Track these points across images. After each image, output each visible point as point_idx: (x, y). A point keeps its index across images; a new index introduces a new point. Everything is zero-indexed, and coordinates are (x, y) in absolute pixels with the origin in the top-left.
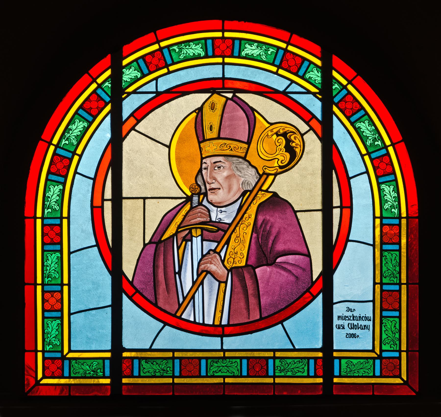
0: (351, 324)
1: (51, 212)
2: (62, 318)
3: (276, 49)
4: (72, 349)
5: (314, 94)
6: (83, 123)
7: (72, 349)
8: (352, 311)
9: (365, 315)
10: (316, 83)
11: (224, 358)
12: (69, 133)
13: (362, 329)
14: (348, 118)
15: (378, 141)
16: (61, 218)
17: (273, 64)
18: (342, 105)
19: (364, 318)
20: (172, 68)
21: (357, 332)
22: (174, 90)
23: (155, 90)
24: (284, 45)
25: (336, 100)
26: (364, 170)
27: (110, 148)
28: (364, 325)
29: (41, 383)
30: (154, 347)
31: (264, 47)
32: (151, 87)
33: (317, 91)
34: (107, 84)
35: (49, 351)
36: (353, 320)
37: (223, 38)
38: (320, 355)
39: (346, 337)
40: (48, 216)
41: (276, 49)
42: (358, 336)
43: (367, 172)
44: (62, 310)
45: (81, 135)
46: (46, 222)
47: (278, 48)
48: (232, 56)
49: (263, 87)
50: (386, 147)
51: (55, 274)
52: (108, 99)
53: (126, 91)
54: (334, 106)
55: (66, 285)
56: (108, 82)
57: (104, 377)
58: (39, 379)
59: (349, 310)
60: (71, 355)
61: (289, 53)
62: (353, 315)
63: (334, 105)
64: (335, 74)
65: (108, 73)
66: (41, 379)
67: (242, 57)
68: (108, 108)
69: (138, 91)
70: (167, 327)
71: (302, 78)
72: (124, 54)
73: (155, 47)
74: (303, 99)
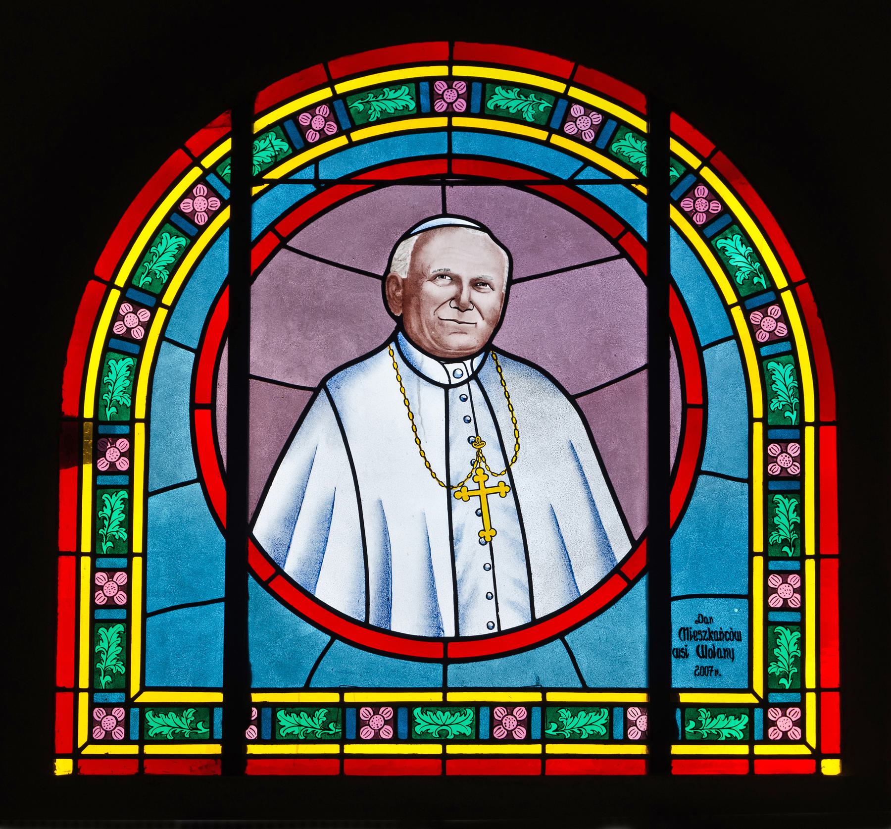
0: (702, 646)
4: (148, 684)
7: (148, 684)
8: (707, 623)
9: (731, 629)
11: (445, 705)
12: (103, 526)
13: (721, 657)
19: (728, 636)
21: (716, 663)
22: (361, 177)
28: (724, 649)
32: (309, 173)
36: (710, 639)
40: (224, 177)
52: (226, 194)
54: (672, 208)
57: (211, 741)
58: (80, 745)
59: (701, 619)
60: (148, 697)
62: (709, 629)
63: (671, 206)
64: (675, 147)
65: (226, 146)
69: (292, 178)
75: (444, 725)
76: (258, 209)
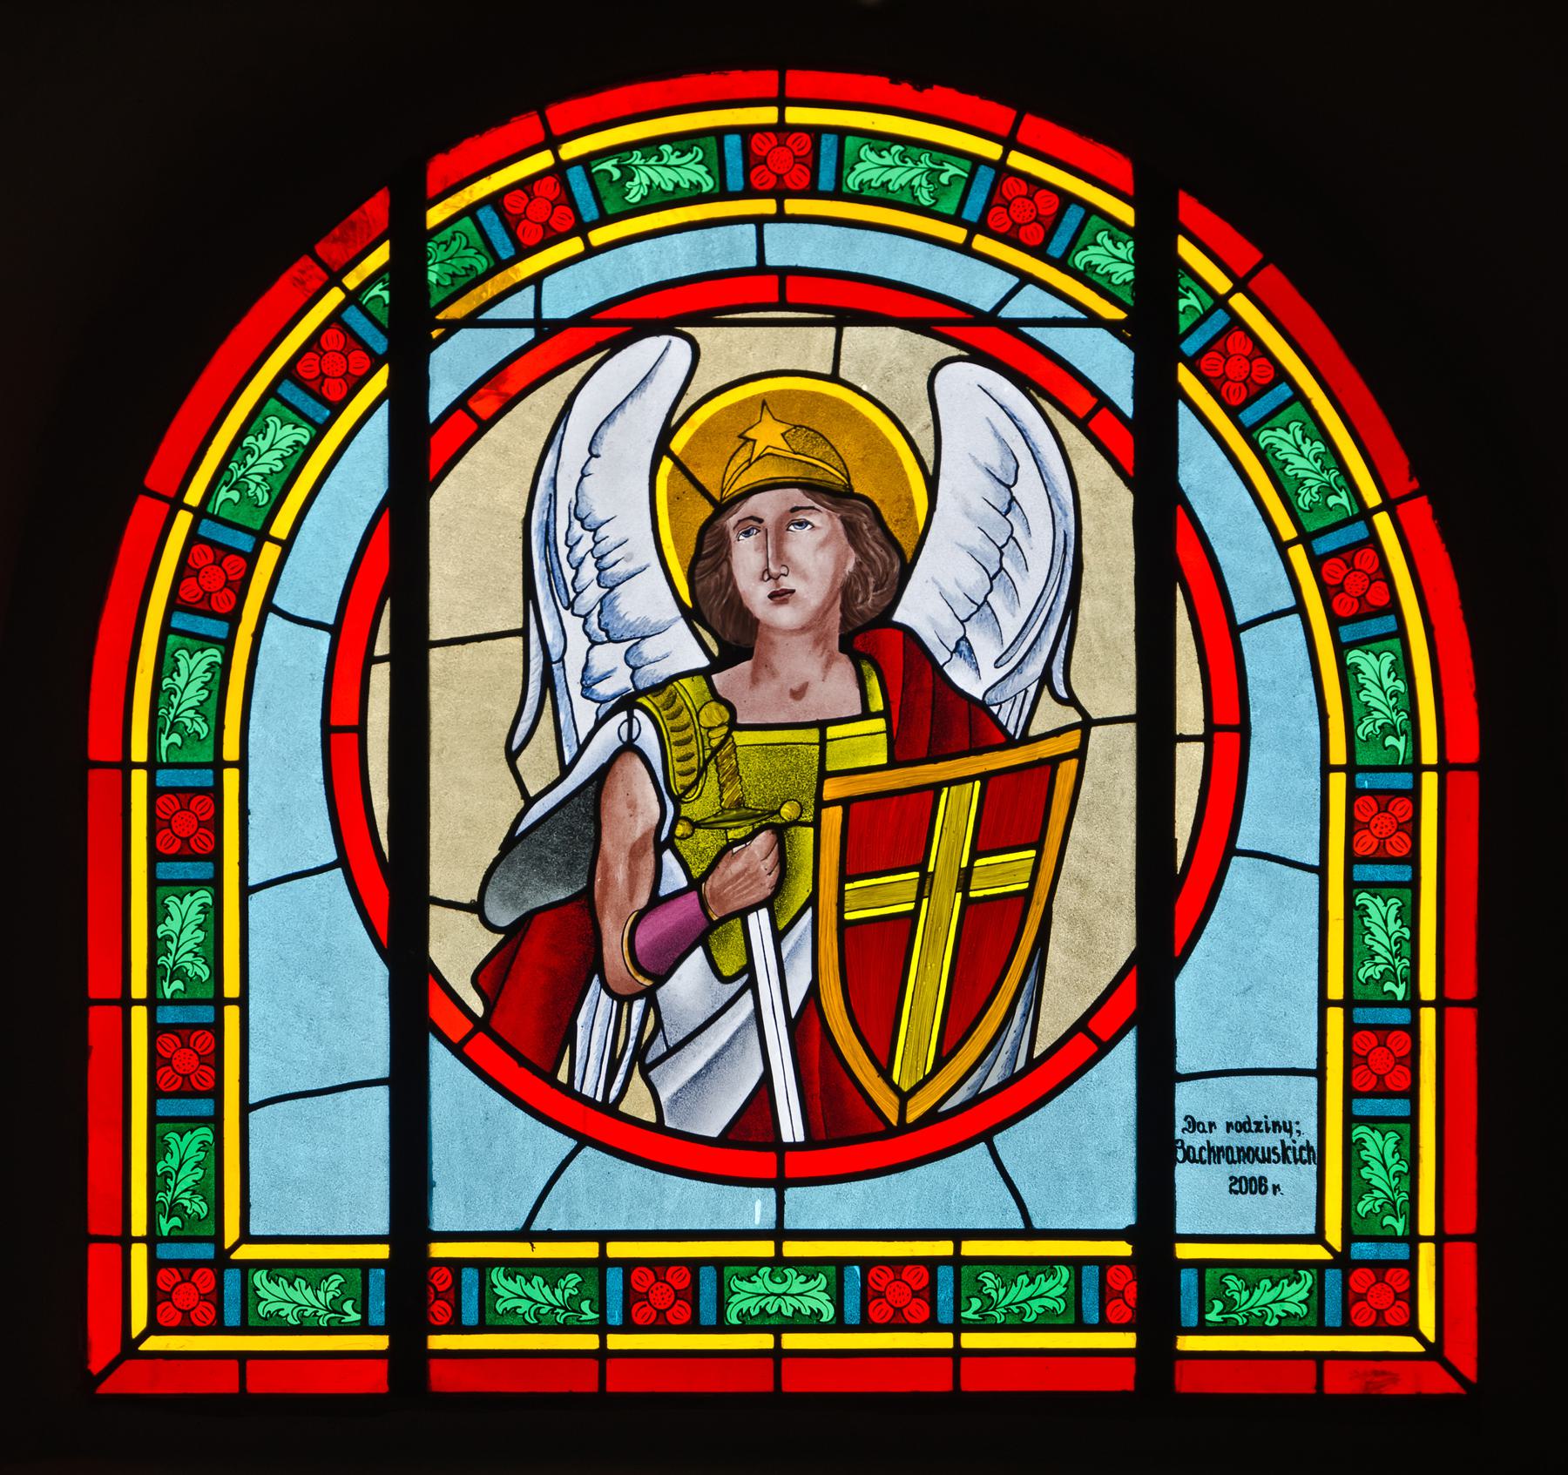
1: (236, 501)
2: (216, 1121)
3: (967, 164)
5: (1112, 327)
6: (294, 428)
10: (1114, 285)
14: (1232, 413)
15: (1337, 494)
16: (218, 765)
17: (956, 220)
18: (1207, 364)
20: (598, 237)
23: (531, 315)
24: (992, 151)
25: (1190, 346)
26: (1289, 601)
27: (386, 516)
29: (143, 1347)
30: (539, 1225)
31: (925, 157)
32: (521, 305)
33: (1120, 315)
34: (376, 291)
35: (170, 1239)
37: (781, 127)
38: (1123, 1249)
39: (1231, 1191)
41: (967, 164)
42: (1276, 1188)
43: (1300, 608)
44: (217, 1094)
45: (539, 1270)
46: (164, 778)
47: (977, 161)
48: (812, 193)
49: (933, 304)
50: (1366, 514)
51: (196, 968)
52: (380, 345)
53: (440, 317)
54: (1181, 367)
55: (231, 1001)
56: (384, 281)
57: (364, 1328)
58: (135, 1333)
61: (1011, 180)
65: (380, 256)
66: (144, 1336)
67: (847, 194)
68: (380, 381)
70: (588, 1151)
71: (1062, 265)
72: (433, 189)
73: (543, 160)
74: (1070, 344)
75: (779, 1296)
76: (440, 361)
